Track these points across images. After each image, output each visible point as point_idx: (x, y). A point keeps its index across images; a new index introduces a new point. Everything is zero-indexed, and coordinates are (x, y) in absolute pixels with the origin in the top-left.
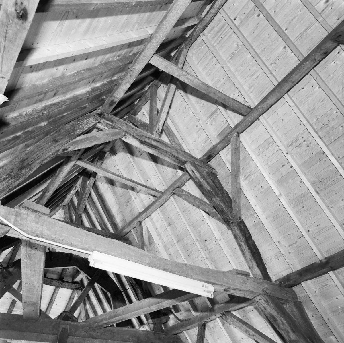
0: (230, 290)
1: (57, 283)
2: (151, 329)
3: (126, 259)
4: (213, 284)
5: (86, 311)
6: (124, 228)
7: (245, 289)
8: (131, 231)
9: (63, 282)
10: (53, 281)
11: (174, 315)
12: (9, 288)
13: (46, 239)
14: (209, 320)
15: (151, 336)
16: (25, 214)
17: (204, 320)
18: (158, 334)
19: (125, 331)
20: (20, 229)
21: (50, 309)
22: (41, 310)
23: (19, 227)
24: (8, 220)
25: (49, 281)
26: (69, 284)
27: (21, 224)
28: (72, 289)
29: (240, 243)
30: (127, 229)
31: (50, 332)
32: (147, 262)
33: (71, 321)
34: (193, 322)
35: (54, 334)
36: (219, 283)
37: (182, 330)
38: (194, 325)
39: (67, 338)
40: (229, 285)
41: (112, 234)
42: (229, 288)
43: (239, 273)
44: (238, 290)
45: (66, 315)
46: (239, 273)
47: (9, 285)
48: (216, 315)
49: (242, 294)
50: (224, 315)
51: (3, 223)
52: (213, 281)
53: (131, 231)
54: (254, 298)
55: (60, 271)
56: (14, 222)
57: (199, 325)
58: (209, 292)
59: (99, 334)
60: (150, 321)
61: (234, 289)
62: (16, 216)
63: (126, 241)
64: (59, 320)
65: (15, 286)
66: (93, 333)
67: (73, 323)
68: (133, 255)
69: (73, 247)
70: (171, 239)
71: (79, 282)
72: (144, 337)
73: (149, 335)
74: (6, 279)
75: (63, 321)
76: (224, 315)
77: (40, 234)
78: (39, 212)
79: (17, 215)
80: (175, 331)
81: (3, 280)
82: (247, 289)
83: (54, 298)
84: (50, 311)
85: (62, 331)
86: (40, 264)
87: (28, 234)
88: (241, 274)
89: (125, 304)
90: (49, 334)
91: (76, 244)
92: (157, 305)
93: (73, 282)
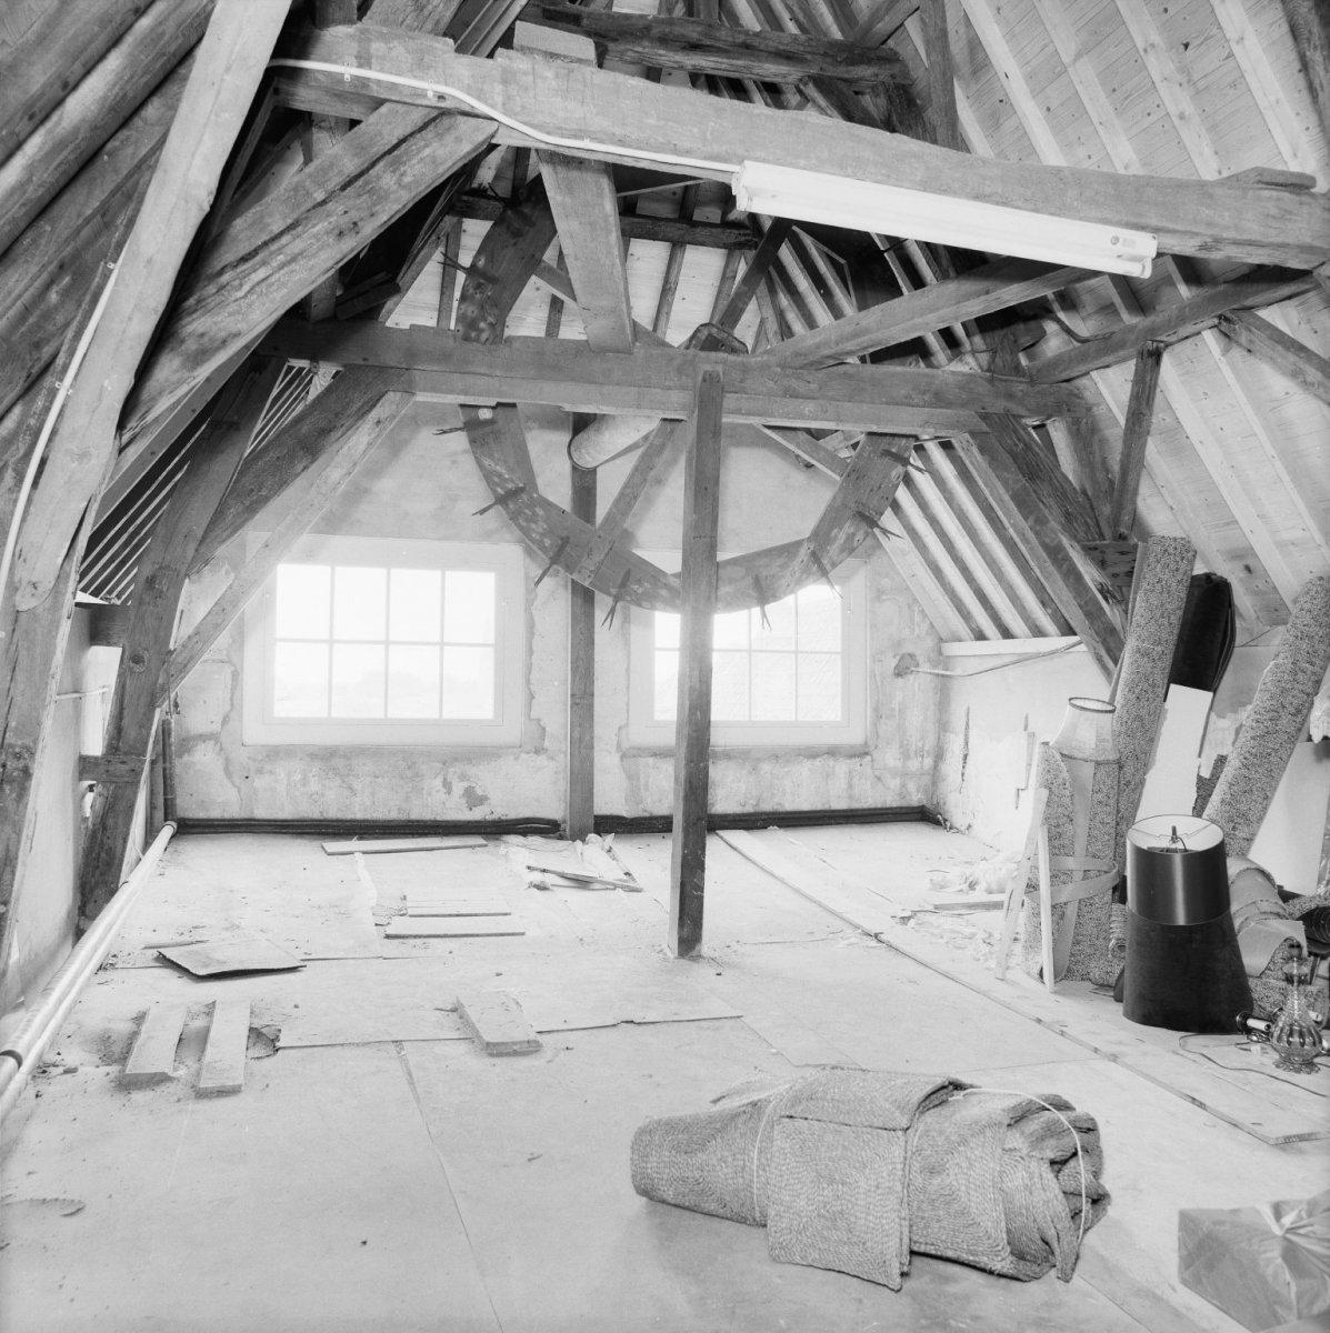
0: (1220, 246)
1: (676, 230)
2: (981, 368)
3: (848, 176)
4: (1156, 230)
5: (780, 315)
6: (876, 16)
7: (1279, 240)
8: (902, 24)
9: (695, 224)
10: (660, 226)
11: (1059, 321)
12: (533, 265)
13: (602, 141)
14: (1173, 338)
15: (981, 389)
16: (525, 73)
17: (1159, 338)
18: (1006, 381)
19: (893, 375)
20: (525, 124)
21: (668, 314)
22: (635, 324)
23: (519, 118)
24: (486, 103)
25: (649, 225)
26: (714, 230)
27: (523, 107)
28: (725, 246)
29: (1308, 53)
30: (887, 18)
31: (671, 384)
32: (919, 178)
33: (725, 351)
34: (1122, 345)
35: (683, 388)
36: (1179, 227)
37: (1083, 369)
38: (1122, 353)
39: (722, 397)
40: (1215, 232)
41: (834, 44)
42: (1218, 240)
43: (1267, 183)
44: (1251, 243)
45: (710, 335)
46: (1267, 183)
47: (533, 256)
48: (1199, 320)
49: (1269, 255)
50: (1227, 320)
51: (476, 112)
52: (1154, 222)
53: (902, 24)
54: (1318, 266)
55: (680, 192)
56: (504, 104)
57: (1141, 355)
58: (1134, 259)
59: (812, 386)
60: (978, 339)
61: (1236, 243)
62: (505, 82)
63: (888, 66)
64: (692, 351)
65: (549, 256)
66: (794, 383)
67: (732, 358)
68: (868, 160)
69: (682, 156)
70: (1051, 48)
71: (747, 222)
72: (957, 390)
73: (972, 386)
74: (521, 239)
75: (703, 354)
76: (1227, 320)
77: (580, 130)
78: (565, 57)
79: (507, 78)
80: (1061, 372)
81: (513, 241)
82: (1287, 241)
83: (672, 279)
84: (668, 319)
85: (704, 380)
86: (602, 205)
87: (548, 133)
88: (1277, 185)
89: (896, 292)
90: (669, 388)
91: (687, 145)
92: (983, 298)
93: (726, 224)
